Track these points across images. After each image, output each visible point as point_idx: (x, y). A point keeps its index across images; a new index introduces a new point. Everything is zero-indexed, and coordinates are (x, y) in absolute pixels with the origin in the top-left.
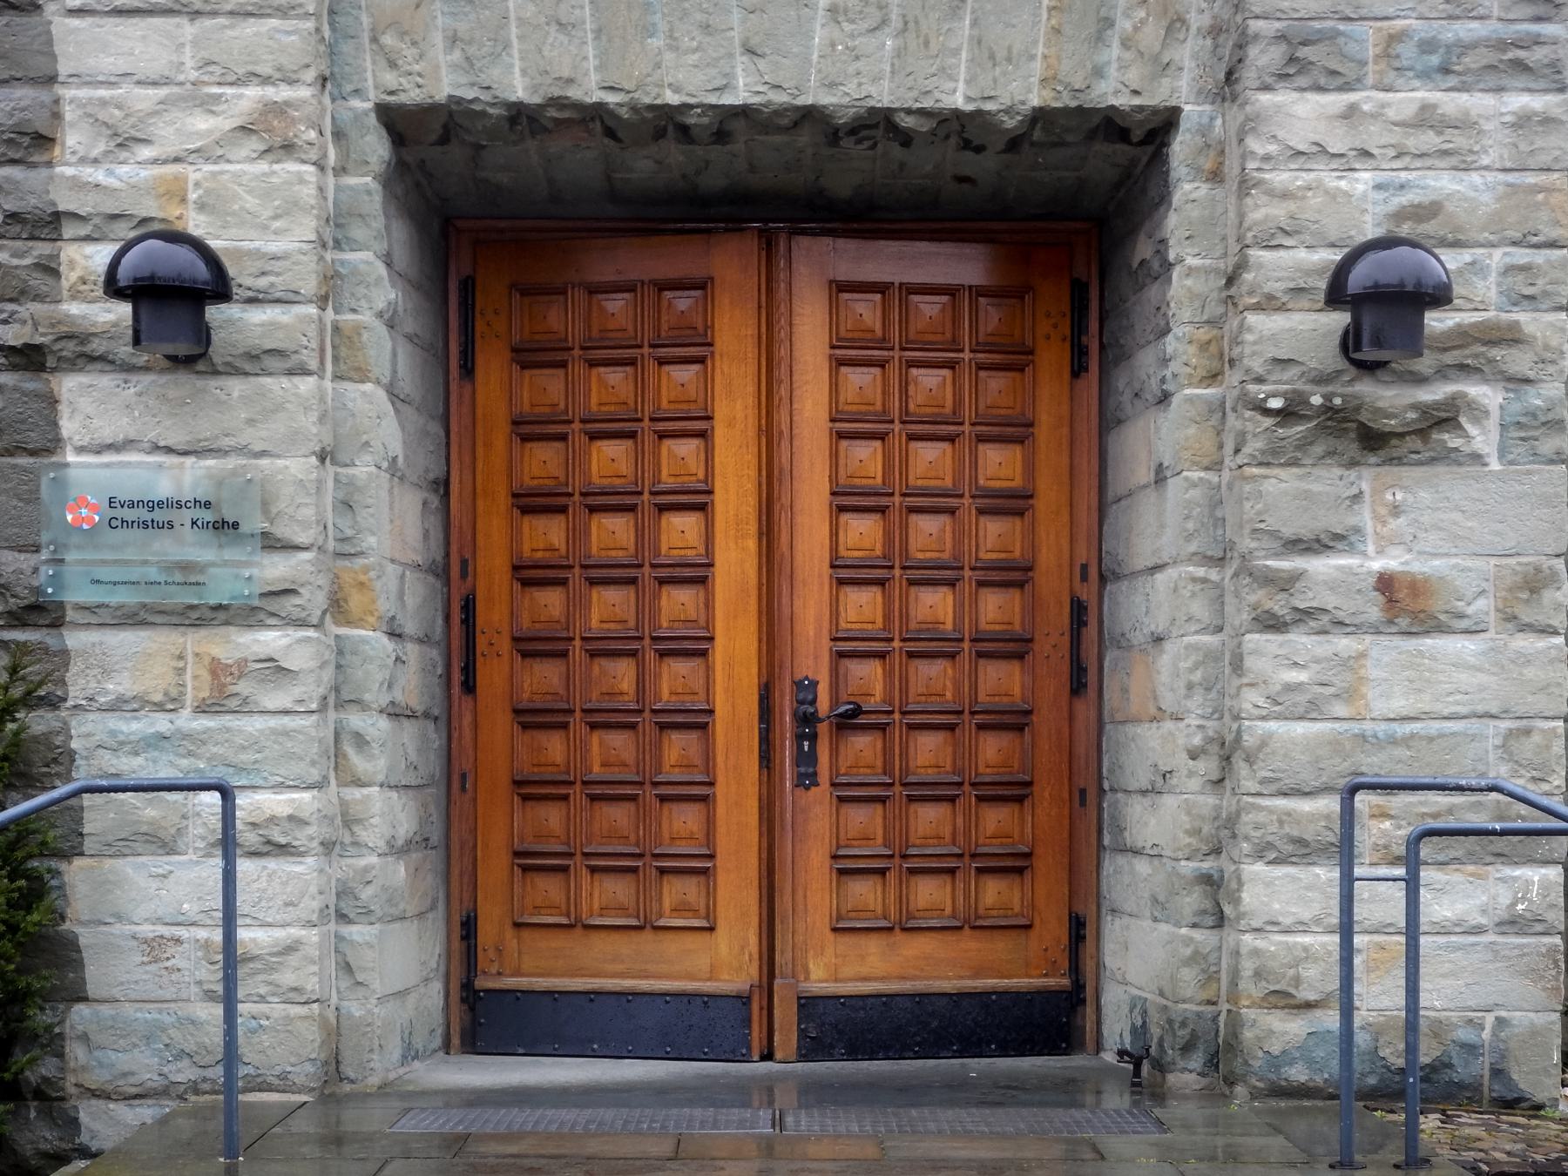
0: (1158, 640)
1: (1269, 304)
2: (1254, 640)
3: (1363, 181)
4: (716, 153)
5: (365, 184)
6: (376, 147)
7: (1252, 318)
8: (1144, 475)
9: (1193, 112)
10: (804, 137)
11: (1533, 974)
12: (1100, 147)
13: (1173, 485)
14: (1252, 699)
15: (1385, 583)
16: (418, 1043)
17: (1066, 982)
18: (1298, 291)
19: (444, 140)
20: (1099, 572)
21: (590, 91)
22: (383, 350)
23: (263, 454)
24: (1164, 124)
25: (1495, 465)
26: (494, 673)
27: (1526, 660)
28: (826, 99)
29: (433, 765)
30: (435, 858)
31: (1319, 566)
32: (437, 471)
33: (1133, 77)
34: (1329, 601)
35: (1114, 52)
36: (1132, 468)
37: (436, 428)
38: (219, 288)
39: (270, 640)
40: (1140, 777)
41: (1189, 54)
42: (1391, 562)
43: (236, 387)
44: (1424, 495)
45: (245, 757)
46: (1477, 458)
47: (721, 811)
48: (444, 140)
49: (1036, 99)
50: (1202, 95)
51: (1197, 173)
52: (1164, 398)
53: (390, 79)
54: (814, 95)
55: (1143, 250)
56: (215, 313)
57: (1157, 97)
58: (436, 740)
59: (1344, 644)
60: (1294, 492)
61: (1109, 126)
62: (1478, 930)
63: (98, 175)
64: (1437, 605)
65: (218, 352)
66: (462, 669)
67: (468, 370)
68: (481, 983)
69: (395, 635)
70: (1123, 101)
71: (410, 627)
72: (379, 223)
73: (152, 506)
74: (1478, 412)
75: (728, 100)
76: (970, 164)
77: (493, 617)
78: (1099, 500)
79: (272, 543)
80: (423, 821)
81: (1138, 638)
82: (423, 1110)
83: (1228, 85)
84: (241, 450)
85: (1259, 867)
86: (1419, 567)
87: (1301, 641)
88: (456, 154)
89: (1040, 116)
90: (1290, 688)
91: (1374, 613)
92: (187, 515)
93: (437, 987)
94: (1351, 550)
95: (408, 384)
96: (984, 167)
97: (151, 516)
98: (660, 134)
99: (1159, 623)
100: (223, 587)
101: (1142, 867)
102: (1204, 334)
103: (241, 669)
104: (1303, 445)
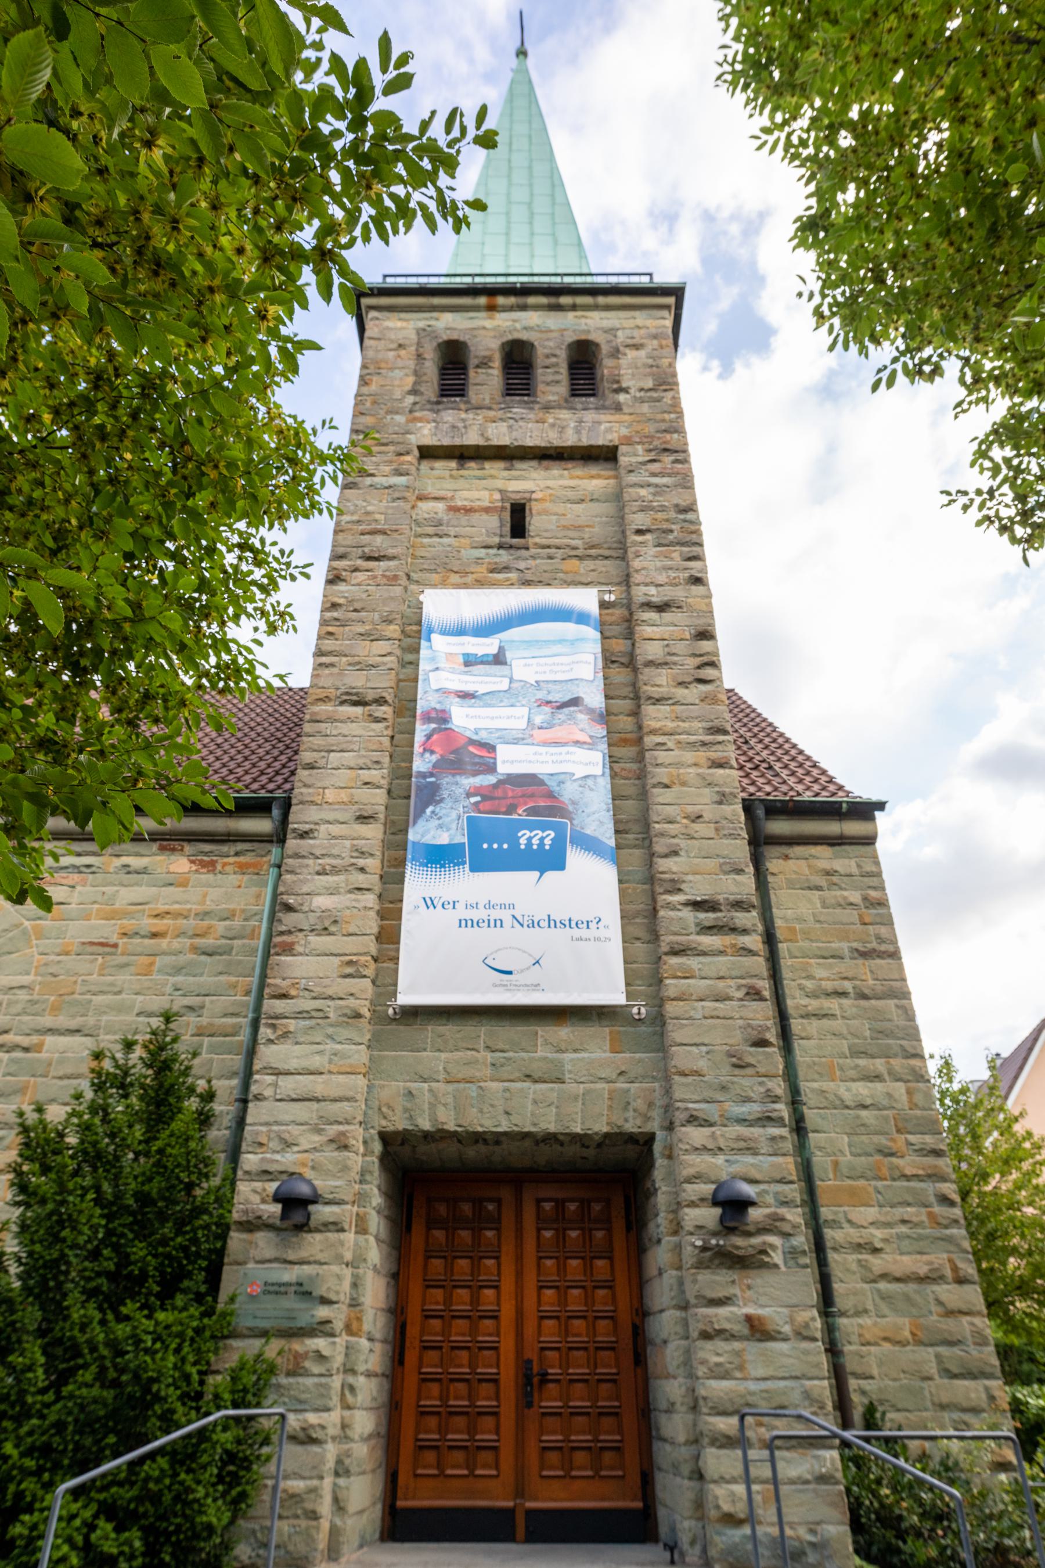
0: (665, 1342)
1: (692, 1204)
2: (700, 1343)
3: (720, 1160)
4: (497, 1148)
5: (374, 1160)
6: (377, 1147)
7: (687, 1210)
8: (655, 1272)
9: (660, 1135)
10: (528, 1143)
11: (833, 1505)
12: (630, 1146)
13: (665, 1276)
14: (701, 1371)
15: (749, 1319)
16: (368, 1537)
17: (639, 1504)
18: (702, 1200)
19: (402, 1144)
20: (642, 1313)
21: (451, 1127)
22: (376, 1223)
23: (892, 1155)
24: (651, 1138)
25: (783, 1268)
26: (411, 1357)
27: (806, 1352)
28: (533, 1129)
29: (384, 1398)
30: (382, 1441)
31: (723, 1311)
32: (394, 1270)
33: (638, 1122)
34: (727, 1326)
35: (630, 1114)
36: (651, 1271)
37: (395, 1253)
38: (315, 1199)
39: (320, 1343)
40: (663, 1405)
41: (656, 1114)
42: (750, 1310)
43: (318, 1237)
44: (759, 1281)
45: (303, 1396)
46: (776, 1266)
47: (502, 1419)
48: (402, 1144)
49: (605, 1129)
50: (663, 1128)
51: (663, 1155)
52: (659, 1241)
53: (384, 1123)
54: (528, 1128)
55: (649, 1185)
56: (312, 1208)
57: (648, 1128)
58: (386, 1385)
59: (737, 1345)
60: (716, 1281)
61: (631, 1139)
62: (807, 1482)
63: (278, 1157)
64: (770, 1327)
65: (312, 1223)
66: (398, 1355)
67: (409, 1228)
68: (400, 1504)
69: (371, 1339)
70: (635, 1130)
71: (378, 1336)
72: (376, 1173)
73: (280, 1285)
74: (773, 1247)
75: (499, 1130)
76: (586, 1152)
77: (413, 1331)
78: (639, 1282)
79: (325, 1301)
80: (377, 1425)
81: (658, 1341)
82: (923, 1458)
83: (670, 1127)
84: (316, 1262)
85: (713, 1450)
86: (760, 1312)
87: (720, 1345)
88: (406, 1150)
89: (607, 1135)
90: (718, 1365)
91: (746, 1331)
92: (293, 1289)
93: (379, 1507)
94: (734, 1304)
95: (384, 1234)
96: (590, 1153)
97: (276, 1290)
98: (477, 1142)
99: (664, 1335)
100: (303, 1321)
101: (668, 1448)
102: (671, 1216)
103: (305, 1356)
104: (711, 1260)
